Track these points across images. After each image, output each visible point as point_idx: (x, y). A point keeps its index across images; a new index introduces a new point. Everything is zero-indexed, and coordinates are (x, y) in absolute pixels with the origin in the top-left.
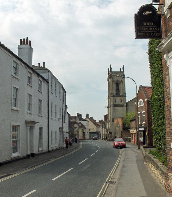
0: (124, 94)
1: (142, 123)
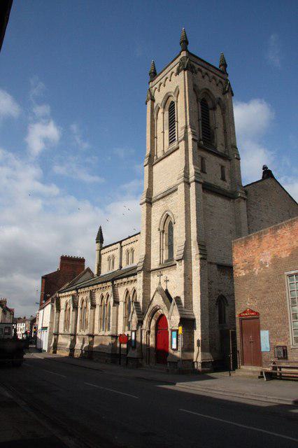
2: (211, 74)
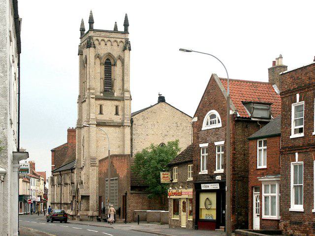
0: (126, 94)
1: (215, 172)
2: (112, 40)
